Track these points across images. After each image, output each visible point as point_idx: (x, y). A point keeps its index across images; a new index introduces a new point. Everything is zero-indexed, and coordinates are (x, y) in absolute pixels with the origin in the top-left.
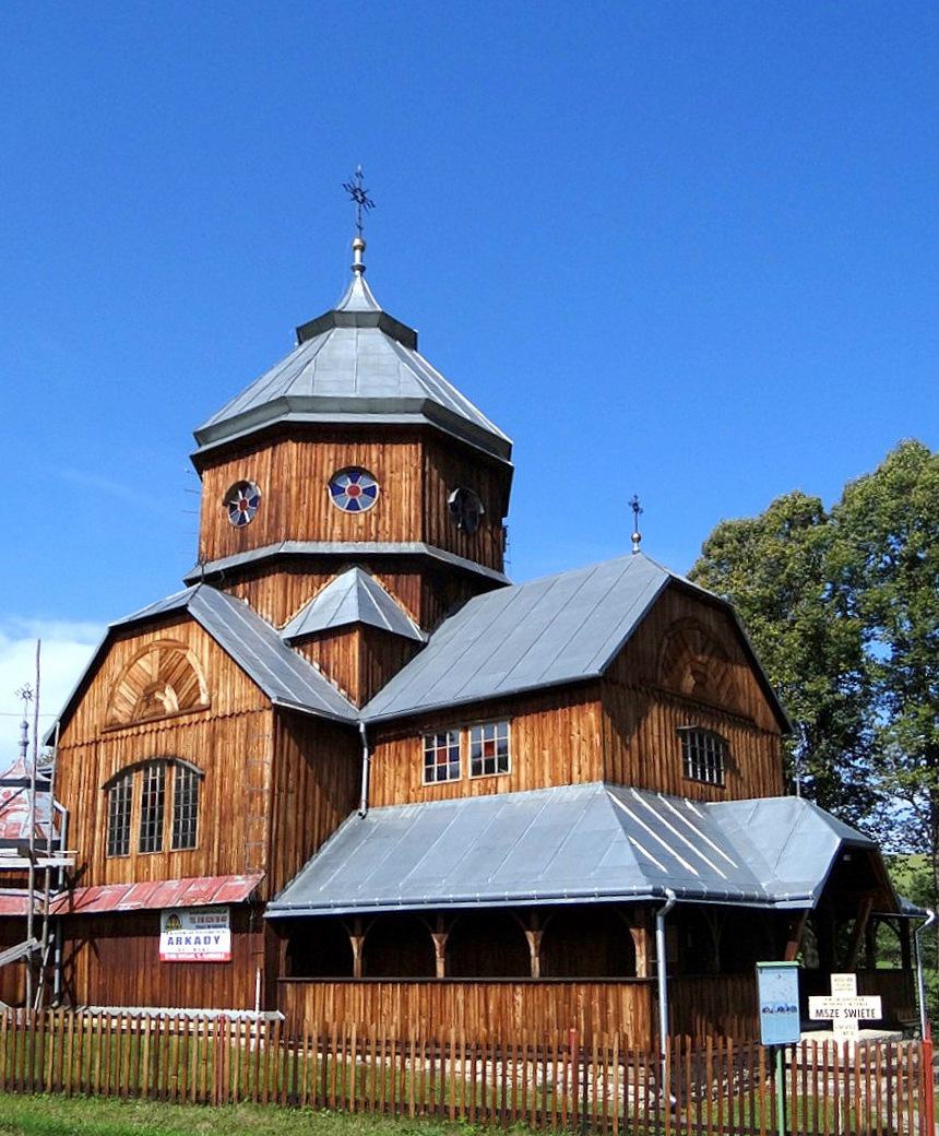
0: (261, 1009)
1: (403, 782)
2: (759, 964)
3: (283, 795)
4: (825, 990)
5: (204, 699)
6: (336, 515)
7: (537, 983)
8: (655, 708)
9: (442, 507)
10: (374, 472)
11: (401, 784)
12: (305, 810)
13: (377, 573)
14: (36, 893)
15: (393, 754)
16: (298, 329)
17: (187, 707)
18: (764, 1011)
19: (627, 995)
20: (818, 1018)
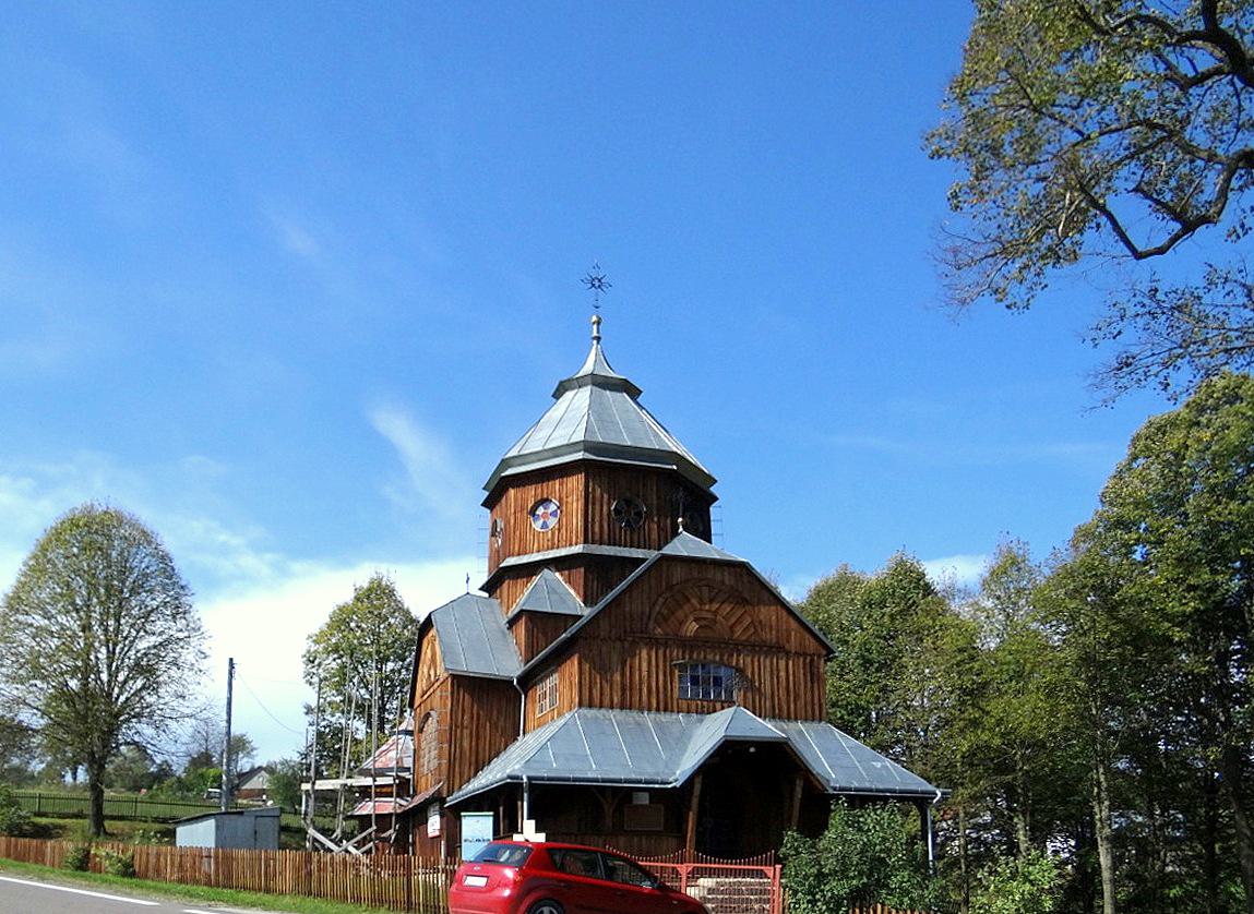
3: (458, 731)
8: (644, 653)
9: (605, 517)
12: (478, 739)
13: (558, 570)
14: (398, 800)
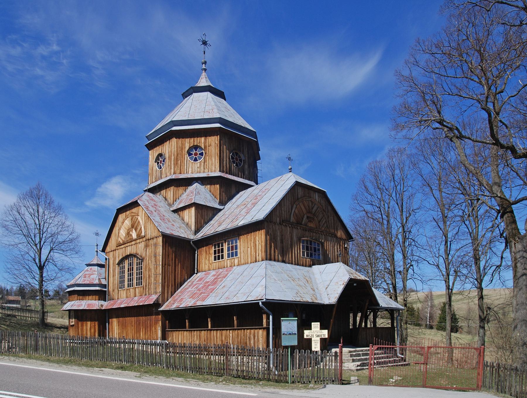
0: (160, 340)
1: (207, 261)
2: (282, 319)
4: (310, 328)
5: (143, 234)
6: (190, 163)
7: (235, 329)
10: (203, 147)
11: (207, 262)
15: (205, 251)
16: (182, 95)
17: (139, 237)
18: (283, 334)
19: (261, 331)
20: (307, 338)
